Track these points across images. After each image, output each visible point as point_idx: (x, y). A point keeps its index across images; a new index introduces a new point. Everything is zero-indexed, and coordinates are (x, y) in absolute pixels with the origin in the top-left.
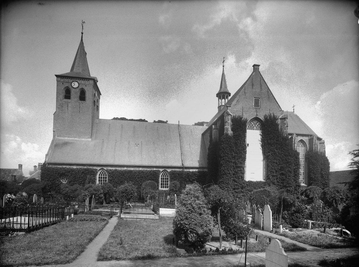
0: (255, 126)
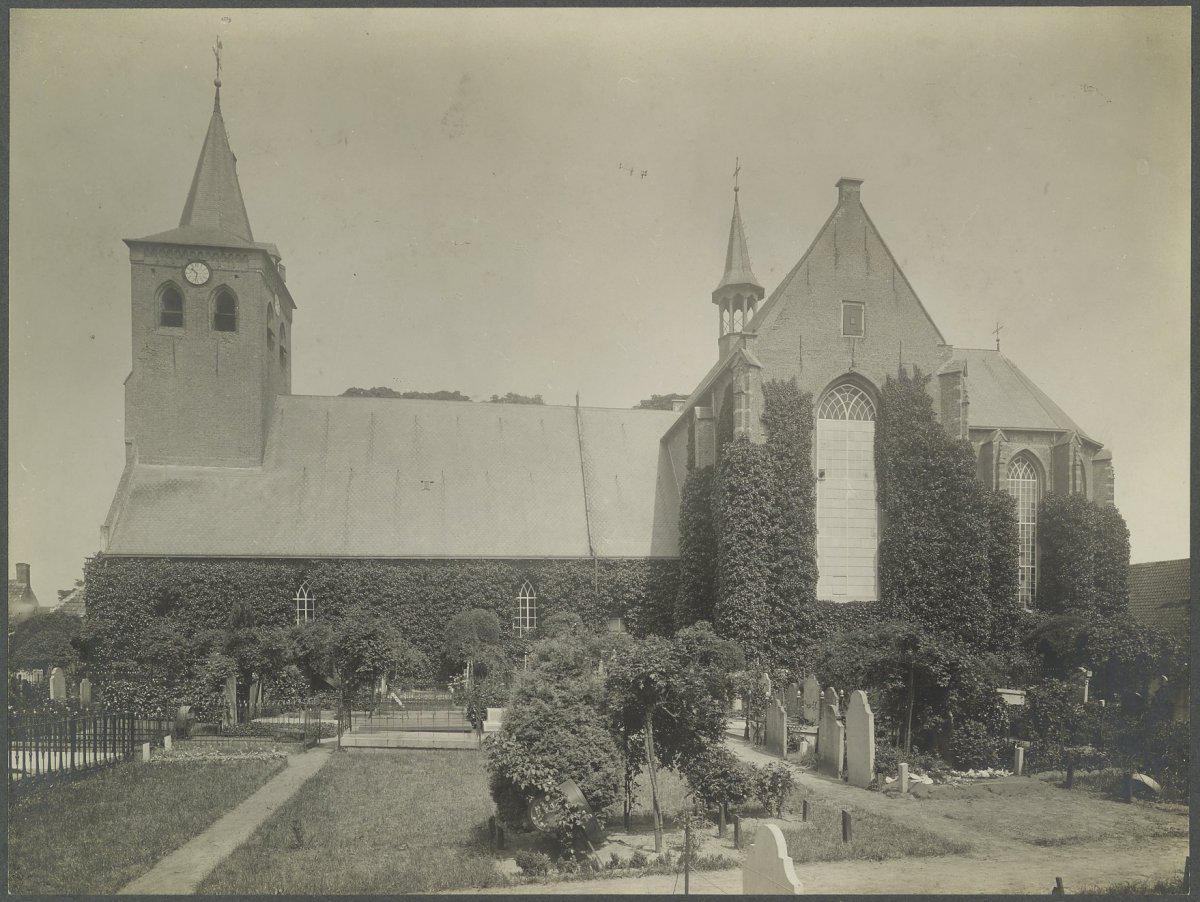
0: (847, 405)
